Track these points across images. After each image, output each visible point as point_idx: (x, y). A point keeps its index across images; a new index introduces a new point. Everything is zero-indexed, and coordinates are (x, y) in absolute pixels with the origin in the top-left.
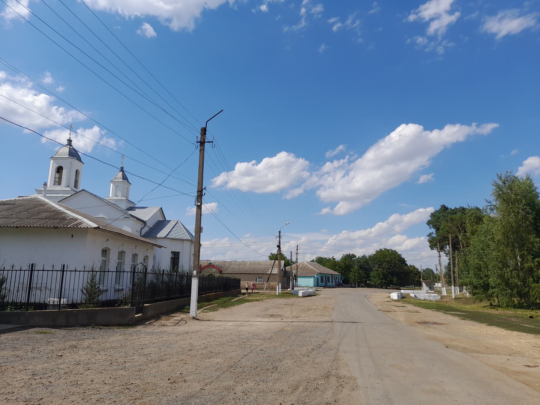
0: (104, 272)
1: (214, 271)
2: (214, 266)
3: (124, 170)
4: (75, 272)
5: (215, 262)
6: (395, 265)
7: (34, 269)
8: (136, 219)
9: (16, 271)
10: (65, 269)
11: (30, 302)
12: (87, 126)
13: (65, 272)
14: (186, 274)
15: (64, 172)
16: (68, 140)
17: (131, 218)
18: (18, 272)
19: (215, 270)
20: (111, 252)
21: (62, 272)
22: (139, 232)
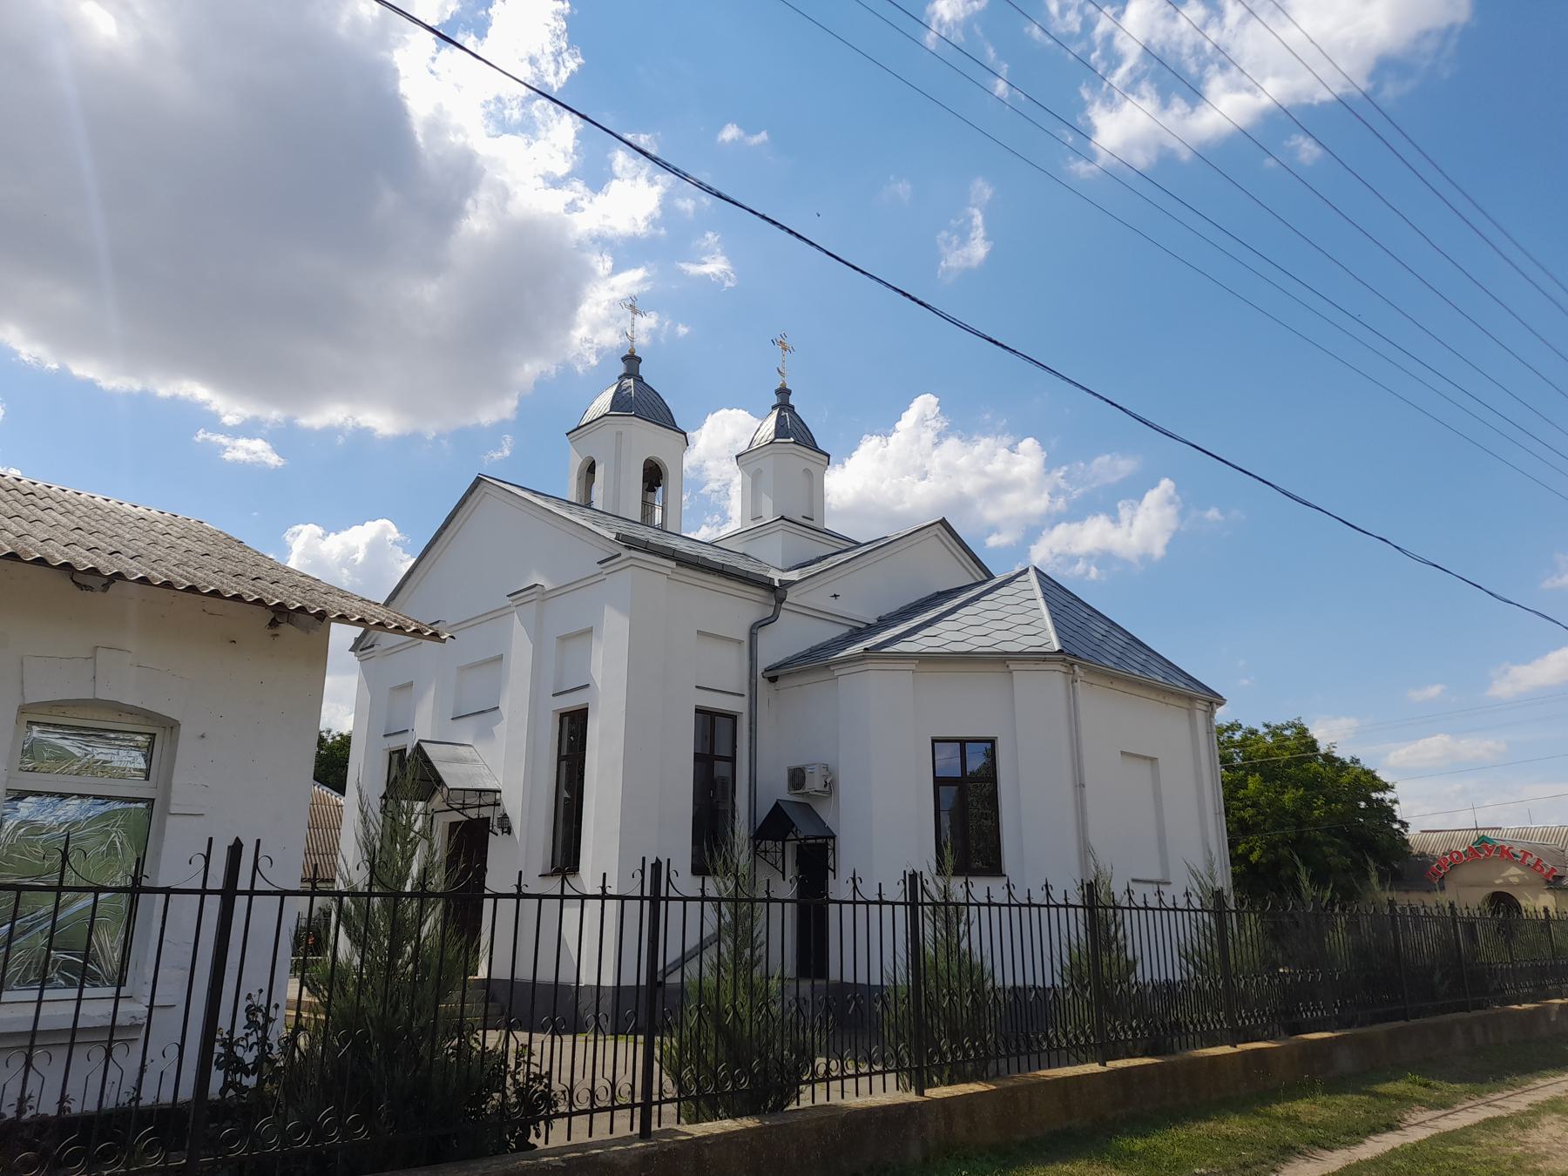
0: (59, 889)
1: (1515, 880)
2: (1506, 854)
3: (791, 403)
4: (198, 897)
5: (1523, 834)
6: (1135, 1018)
7: (663, 894)
8: (673, 564)
9: (536, 901)
10: (243, 883)
11: (641, 1038)
12: (1135, 490)
13: (241, 902)
14: (1543, 914)
15: (600, 471)
16: (624, 359)
17: (626, 553)
18: (1005, 910)
19: (1519, 872)
20: (182, 728)
21: (647, 903)
22: (740, 642)
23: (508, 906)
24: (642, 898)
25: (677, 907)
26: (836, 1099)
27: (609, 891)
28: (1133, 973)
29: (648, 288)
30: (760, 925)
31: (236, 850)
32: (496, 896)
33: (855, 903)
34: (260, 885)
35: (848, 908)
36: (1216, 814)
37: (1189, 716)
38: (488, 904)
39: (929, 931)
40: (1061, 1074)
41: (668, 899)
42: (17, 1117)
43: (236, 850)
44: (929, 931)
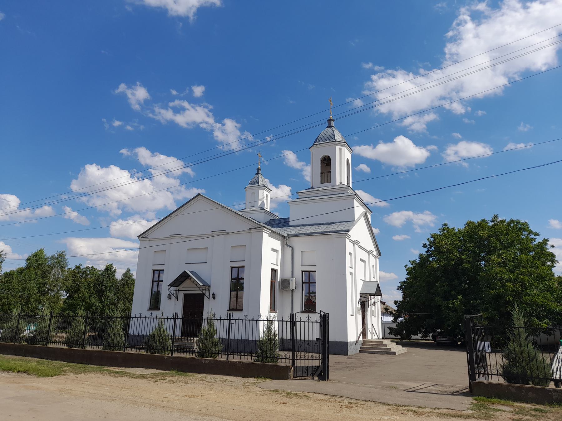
9: (223, 320)
23: (134, 319)
24: (173, 318)
25: (234, 321)
26: (490, 380)
27: (157, 317)
28: (551, 358)
29: (385, 215)
30: (215, 325)
31: (176, 313)
32: (205, 319)
33: (246, 320)
34: (233, 319)
35: (139, 319)
36: (153, 281)
37: (353, 245)
38: (203, 320)
39: (53, 322)
40: (452, 390)
41: (177, 319)
42: (507, 358)
43: (176, 313)
44: (53, 322)
